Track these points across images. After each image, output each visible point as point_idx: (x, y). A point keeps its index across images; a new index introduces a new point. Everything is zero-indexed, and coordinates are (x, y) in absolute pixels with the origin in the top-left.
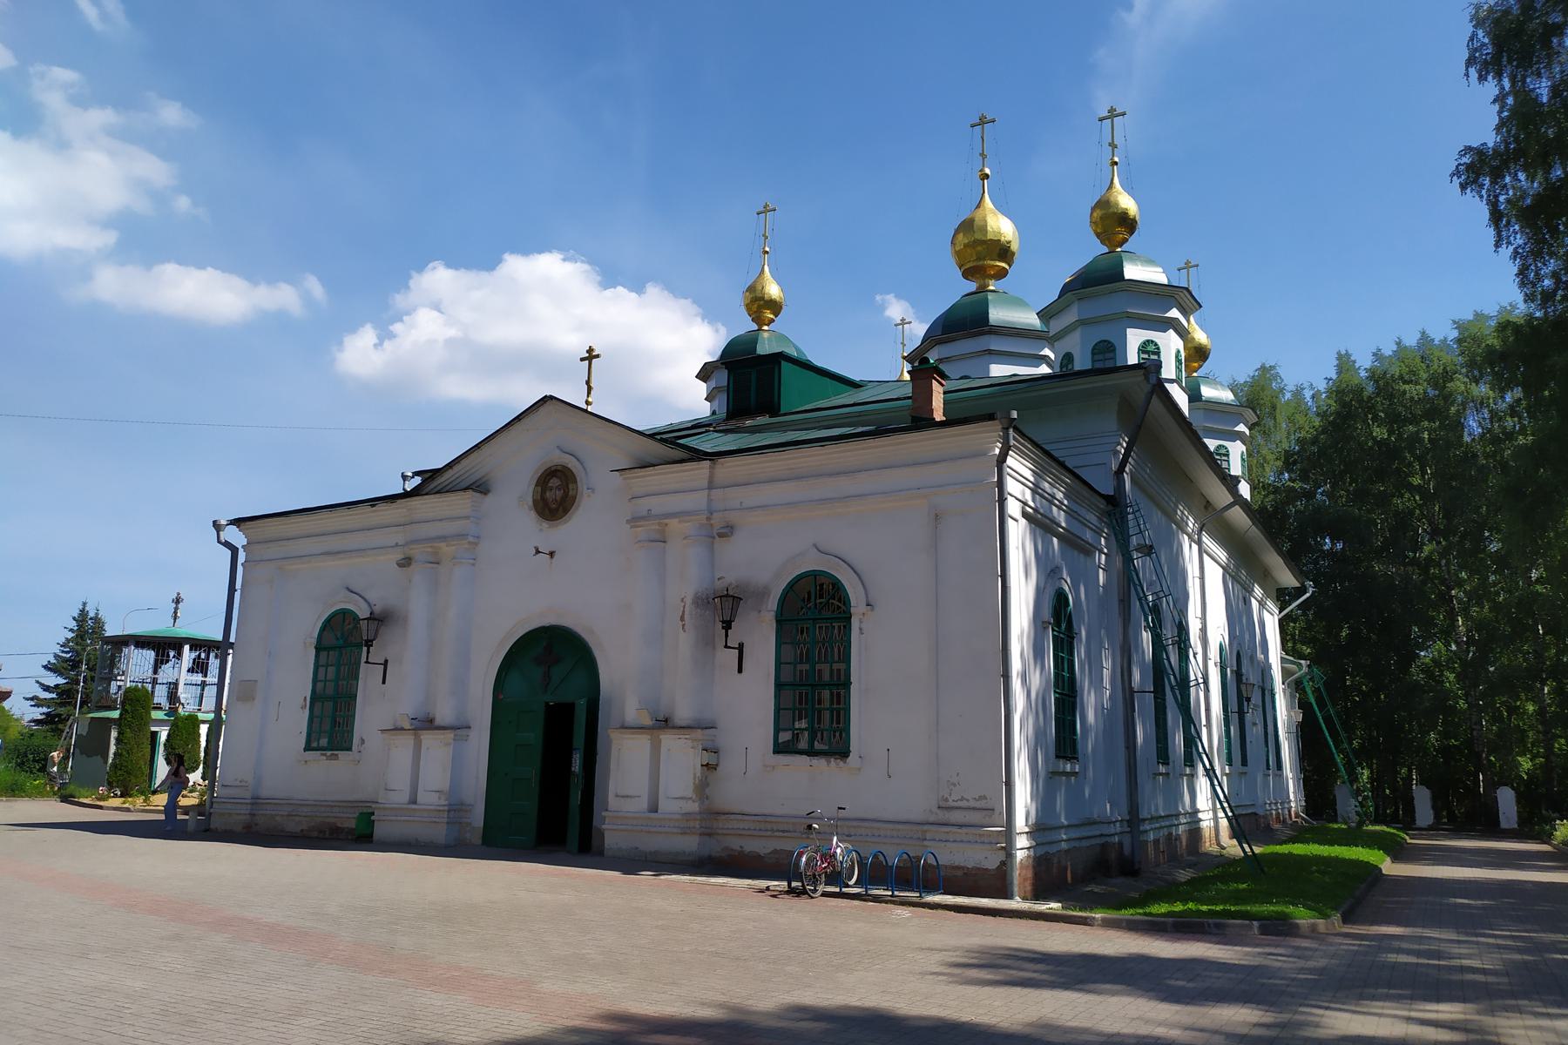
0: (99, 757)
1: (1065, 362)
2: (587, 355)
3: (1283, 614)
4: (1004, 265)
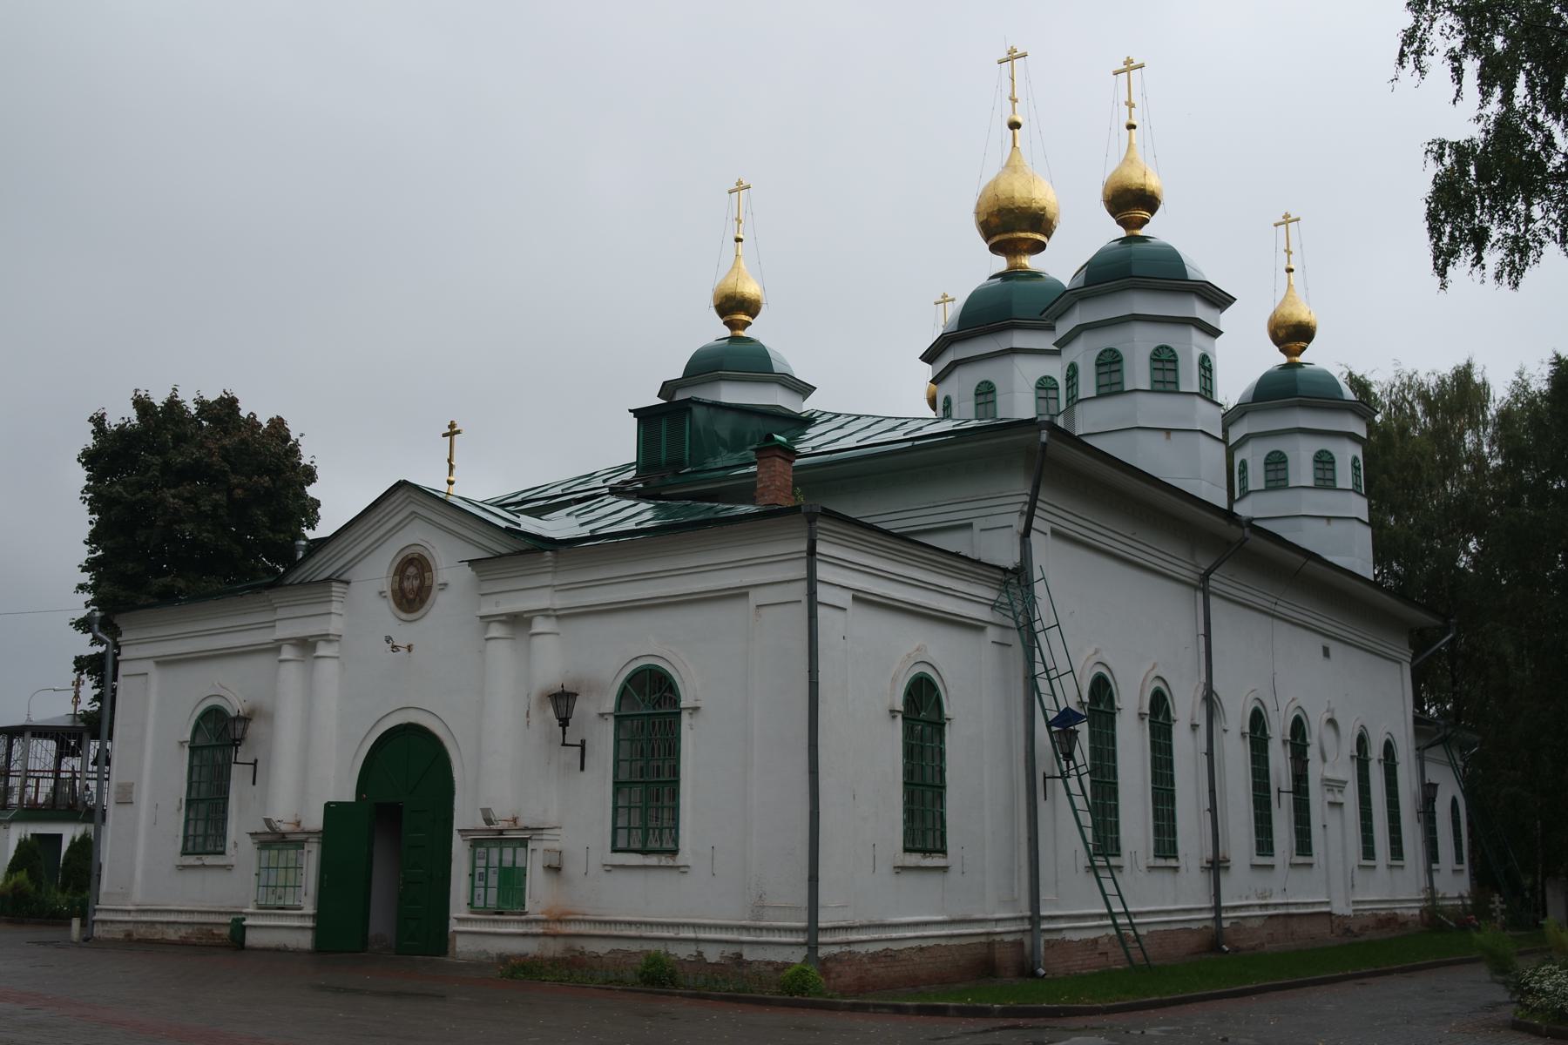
0: (744, 958)
1: (1071, 373)
2: (449, 430)
3: (1417, 661)
4: (1039, 237)
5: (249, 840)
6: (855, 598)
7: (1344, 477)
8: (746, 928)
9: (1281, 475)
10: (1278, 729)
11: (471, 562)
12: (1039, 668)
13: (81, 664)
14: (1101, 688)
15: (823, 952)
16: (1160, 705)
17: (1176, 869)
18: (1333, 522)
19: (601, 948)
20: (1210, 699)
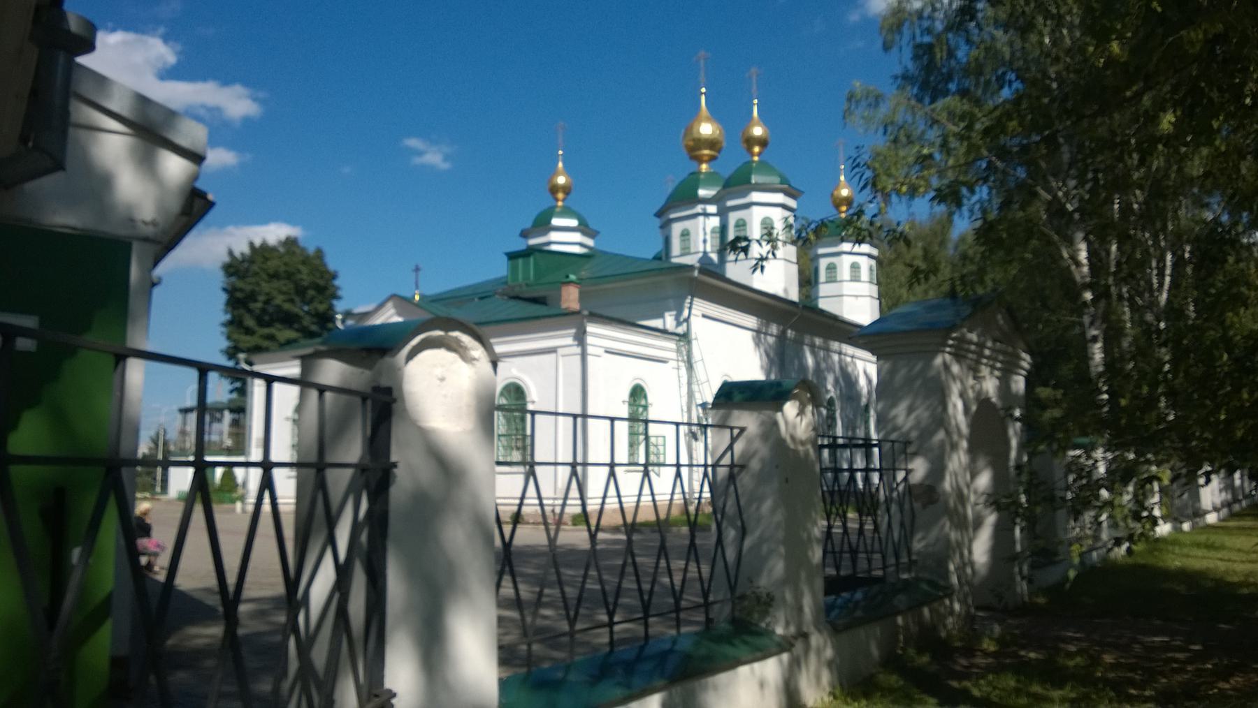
7: (865, 274)
9: (833, 274)
18: (859, 298)
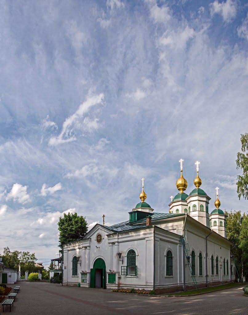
5: (80, 273)
6: (160, 240)
8: (145, 286)
10: (215, 258)
11: (107, 235)
12: (185, 250)
13: (60, 251)
14: (193, 253)
15: (155, 289)
16: (200, 254)
17: (202, 276)
19: (126, 288)
20: (207, 254)
